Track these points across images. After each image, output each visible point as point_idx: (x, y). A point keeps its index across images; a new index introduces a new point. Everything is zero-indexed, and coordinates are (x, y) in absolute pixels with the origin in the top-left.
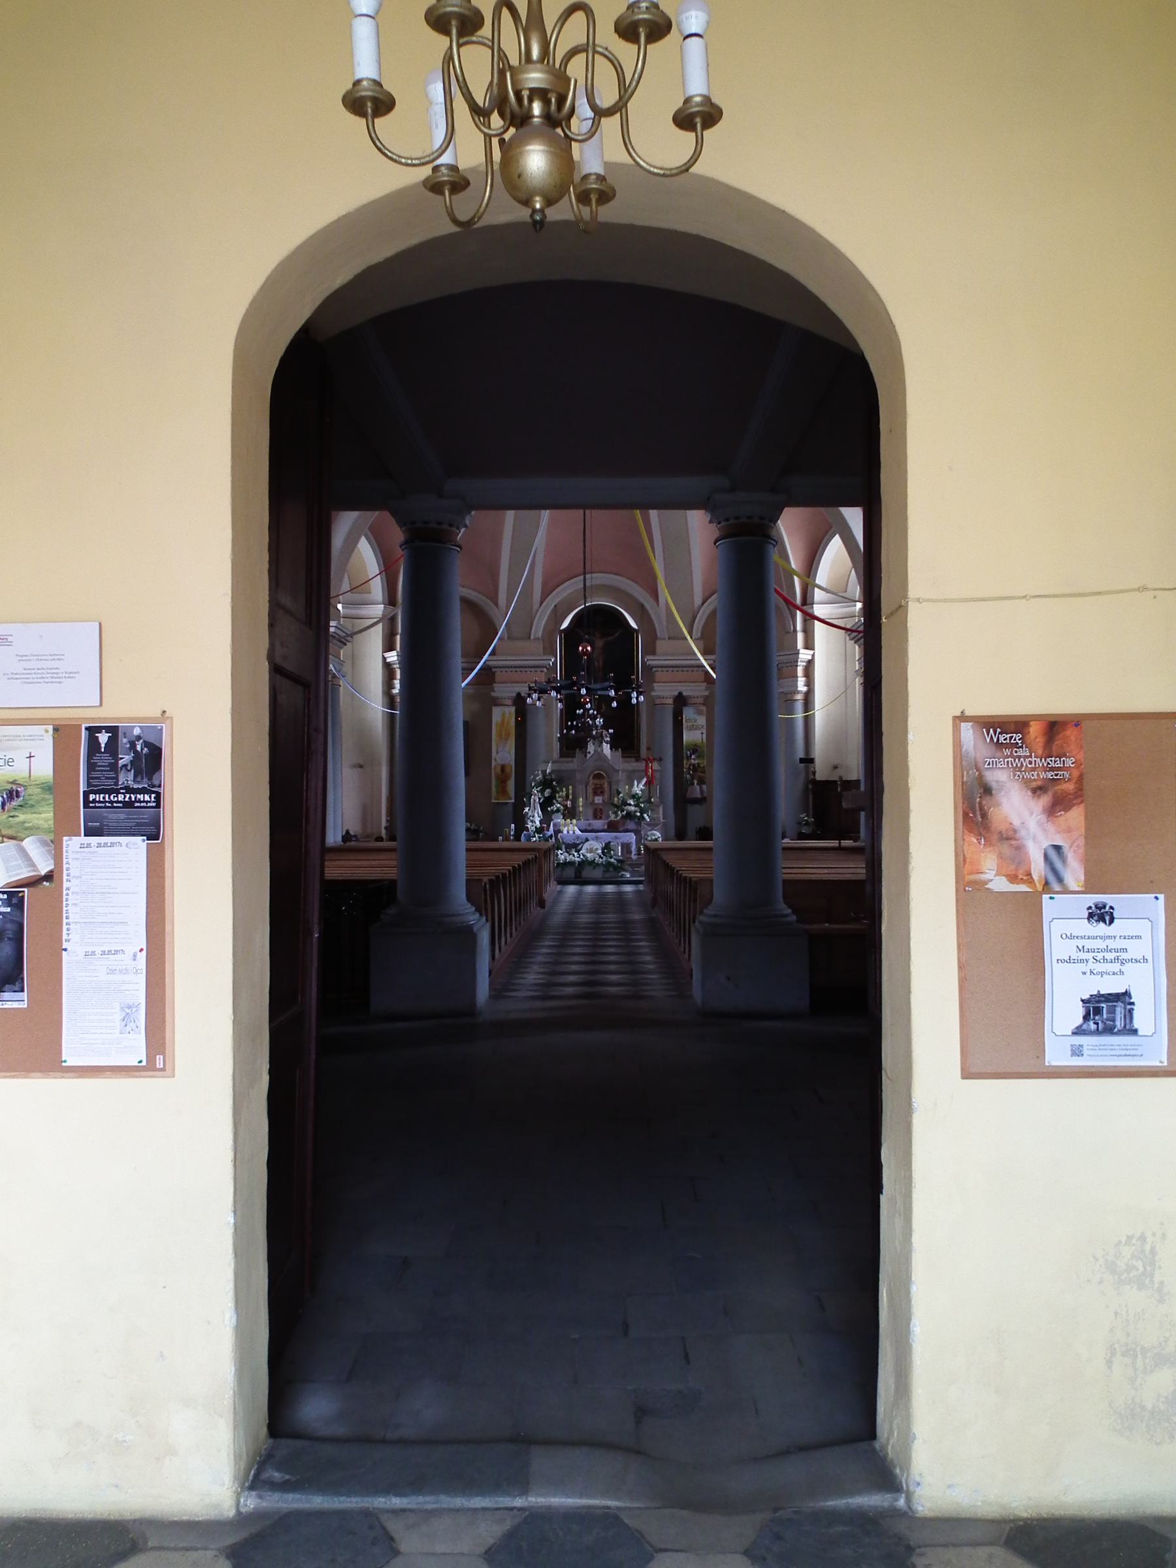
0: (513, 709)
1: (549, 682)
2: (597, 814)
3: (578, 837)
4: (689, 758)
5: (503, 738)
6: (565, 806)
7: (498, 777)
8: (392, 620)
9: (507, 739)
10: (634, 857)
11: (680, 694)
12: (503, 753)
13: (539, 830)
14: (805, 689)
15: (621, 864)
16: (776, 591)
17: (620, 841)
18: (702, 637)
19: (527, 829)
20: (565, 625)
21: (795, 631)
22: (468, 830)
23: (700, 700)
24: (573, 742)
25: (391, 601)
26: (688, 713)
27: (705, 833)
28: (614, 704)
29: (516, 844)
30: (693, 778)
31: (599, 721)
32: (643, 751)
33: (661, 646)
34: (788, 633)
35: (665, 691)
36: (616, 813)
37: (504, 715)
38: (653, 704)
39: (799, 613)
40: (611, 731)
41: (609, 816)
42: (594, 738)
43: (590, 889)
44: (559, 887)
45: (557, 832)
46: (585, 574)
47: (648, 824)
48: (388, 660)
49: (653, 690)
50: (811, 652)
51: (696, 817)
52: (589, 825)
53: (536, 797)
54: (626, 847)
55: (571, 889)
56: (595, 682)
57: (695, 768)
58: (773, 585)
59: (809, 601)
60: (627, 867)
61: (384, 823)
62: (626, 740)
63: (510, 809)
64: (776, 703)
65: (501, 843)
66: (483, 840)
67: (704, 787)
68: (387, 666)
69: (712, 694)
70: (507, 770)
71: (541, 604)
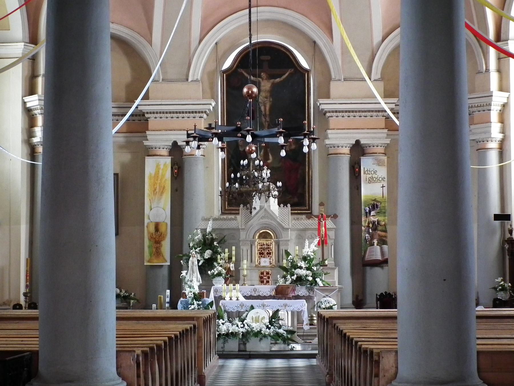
0: (168, 160)
1: (210, 127)
2: (263, 279)
3: (242, 305)
4: (368, 214)
5: (158, 192)
6: (228, 270)
7: (151, 238)
8: (34, 59)
9: (162, 193)
10: (306, 327)
11: (358, 142)
12: (157, 209)
13: (198, 297)
14: (500, 136)
15: (289, 337)
16: (467, 26)
17: (290, 309)
18: (382, 79)
19: (185, 296)
20: (227, 64)
21: (487, 70)
22: (118, 296)
23: (381, 150)
24: (237, 197)
25: (33, 40)
26: (366, 163)
27: (387, 300)
28: (283, 153)
29: (172, 313)
30: (372, 238)
31: (266, 173)
32: (316, 209)
33: (335, 88)
34: (480, 72)
35: (340, 138)
36: (284, 277)
37: (158, 166)
38: (329, 155)
39: (492, 52)
40: (279, 184)
41: (276, 281)
42: (260, 192)
43: (257, 364)
44: (221, 362)
45: (219, 298)
46: (250, 7)
47: (322, 290)
48: (28, 105)
49: (326, 137)
50: (506, 94)
51: (378, 281)
52: (255, 290)
53: (195, 260)
54: (297, 315)
55: (235, 364)
56: (262, 127)
57: (375, 226)
58: (463, 19)
59: (503, 36)
60: (298, 339)
61: (23, 289)
62: (296, 195)
63: (165, 272)
64: (468, 151)
65: (154, 312)
66: (134, 307)
67: (385, 247)
68: (28, 112)
69: (395, 142)
70: (162, 229)
71: (200, 41)
